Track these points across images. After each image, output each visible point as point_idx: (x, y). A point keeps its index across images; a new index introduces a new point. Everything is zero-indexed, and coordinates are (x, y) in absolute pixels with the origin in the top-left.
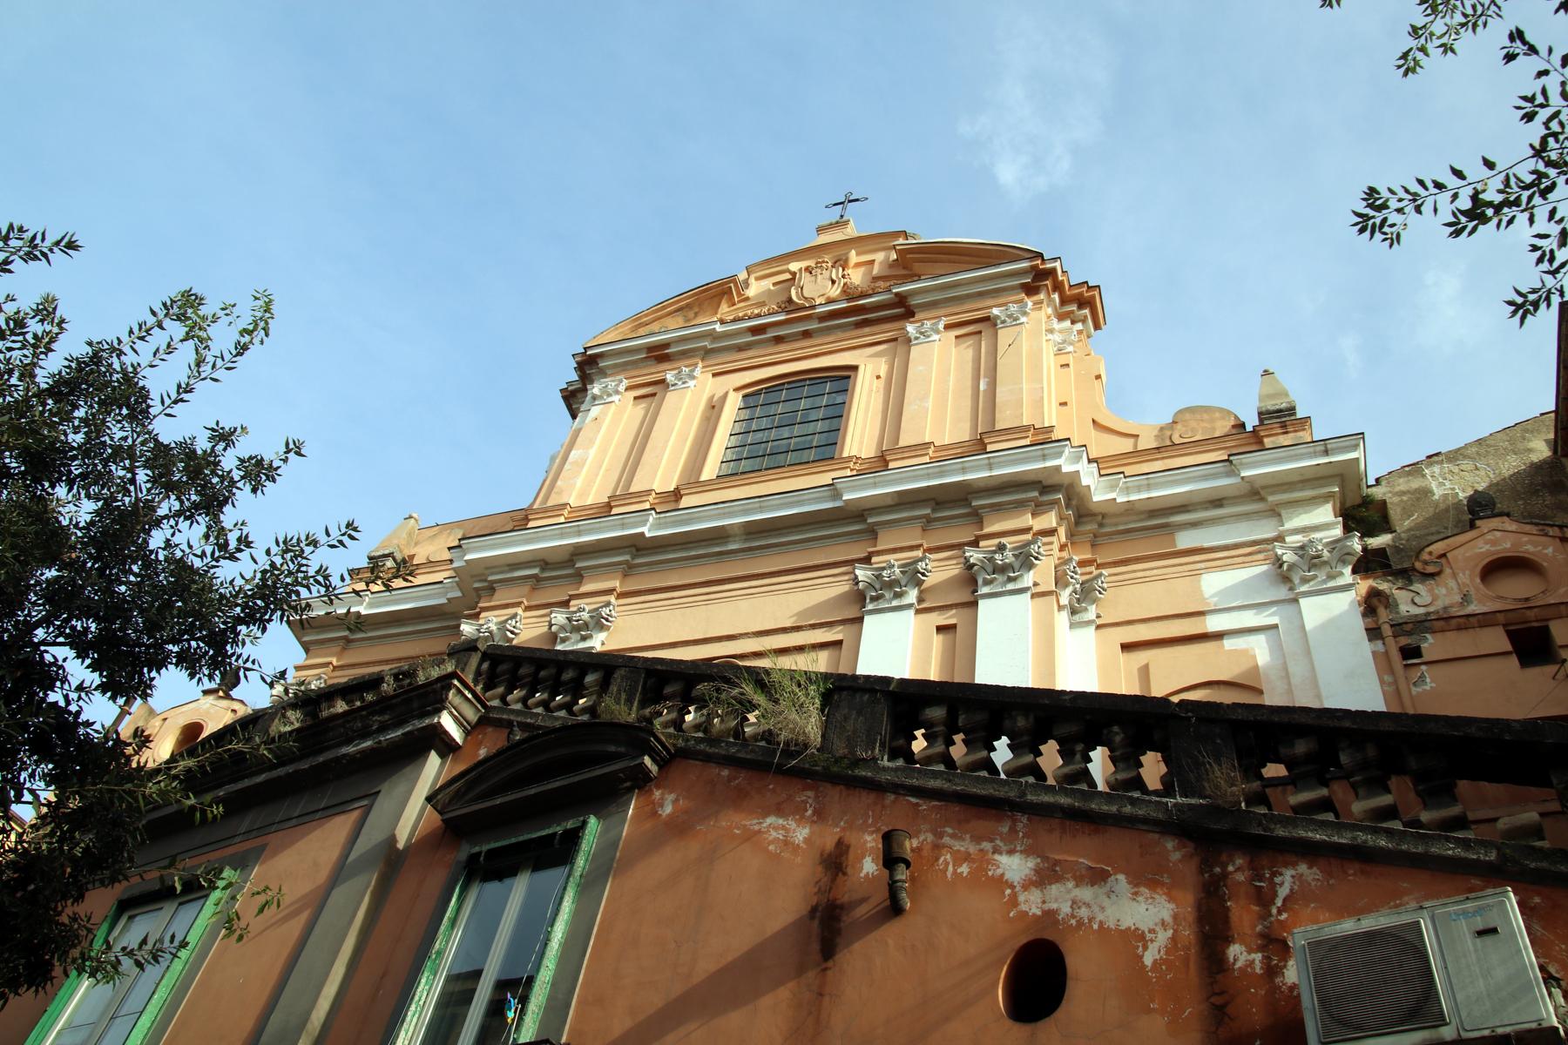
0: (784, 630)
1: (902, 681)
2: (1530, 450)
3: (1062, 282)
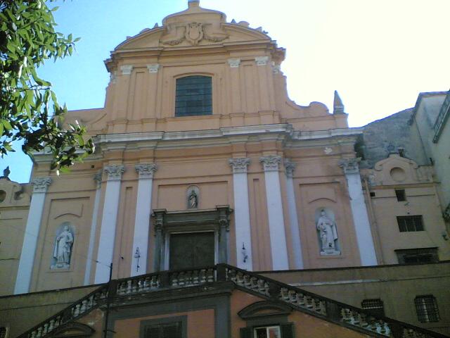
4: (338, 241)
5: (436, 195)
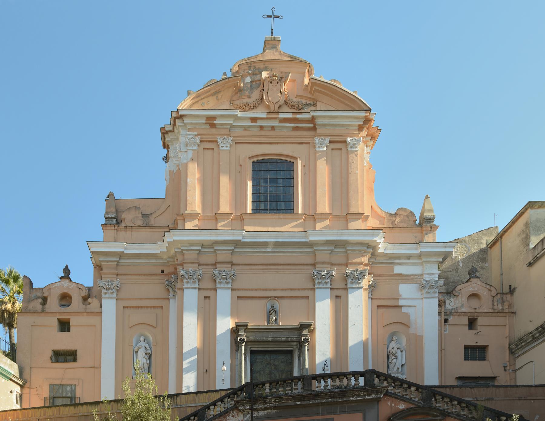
1: (498, 411)
2: (481, 243)
4: (405, 366)
5: (507, 326)
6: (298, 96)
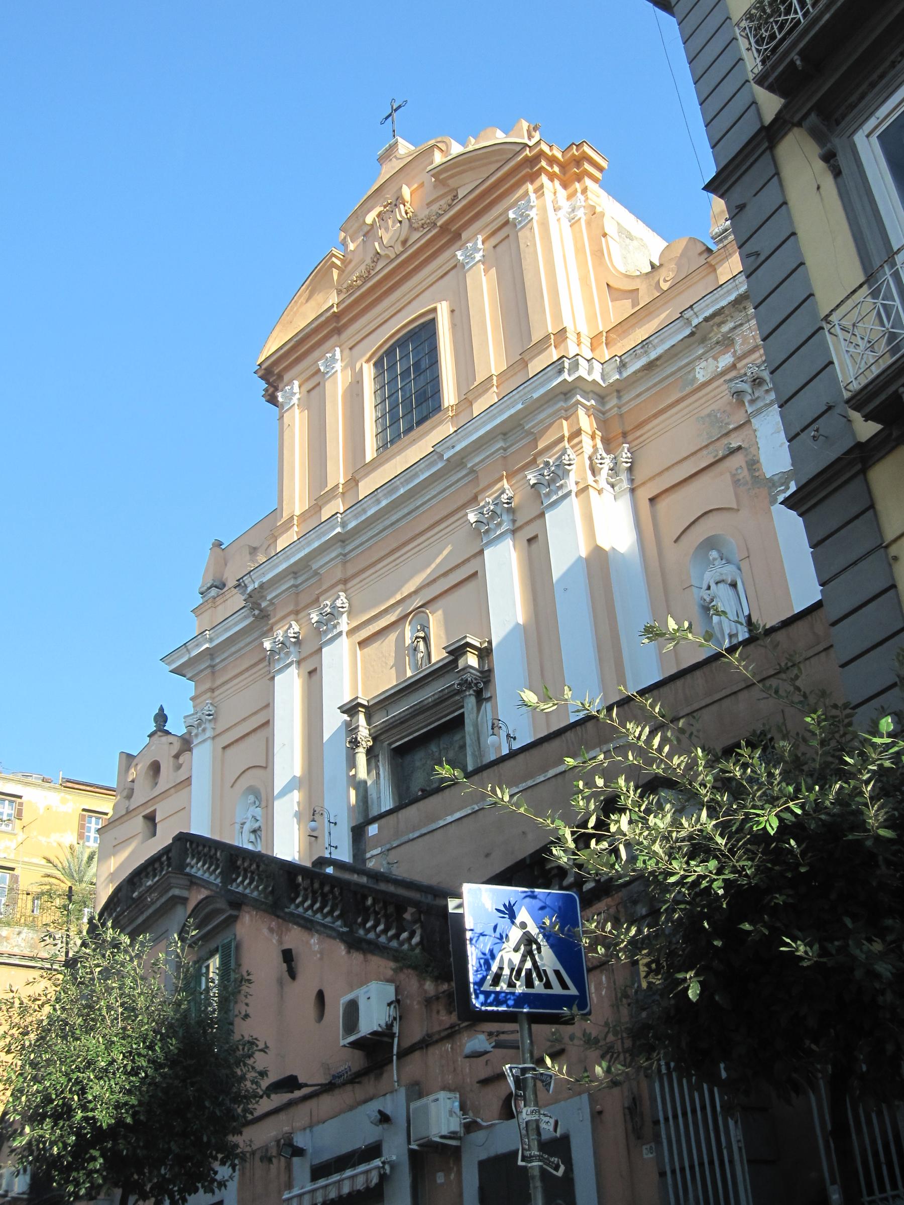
0: (457, 566)
3: (553, 156)
6: (429, 204)
